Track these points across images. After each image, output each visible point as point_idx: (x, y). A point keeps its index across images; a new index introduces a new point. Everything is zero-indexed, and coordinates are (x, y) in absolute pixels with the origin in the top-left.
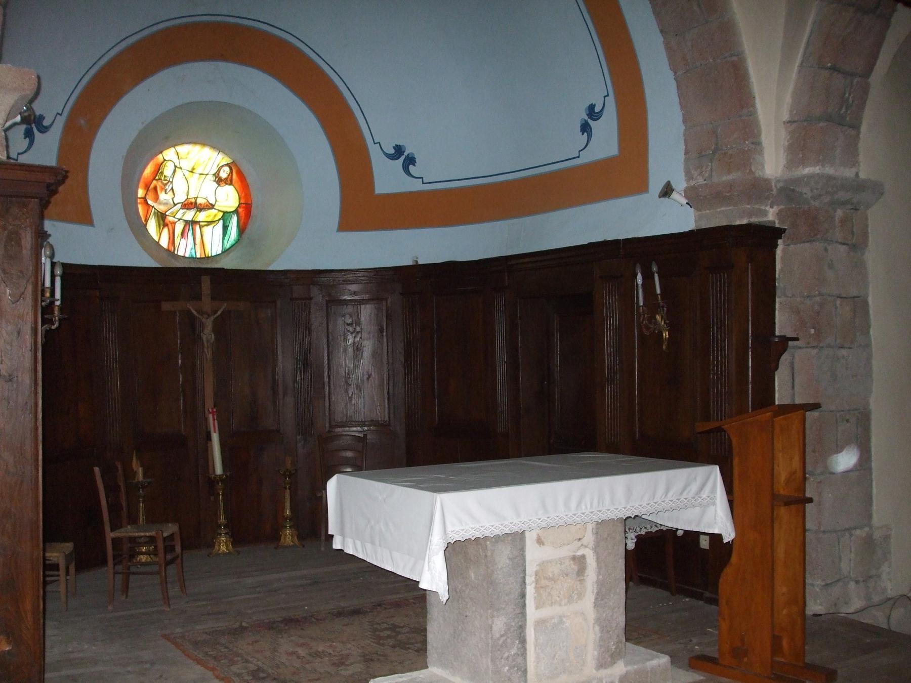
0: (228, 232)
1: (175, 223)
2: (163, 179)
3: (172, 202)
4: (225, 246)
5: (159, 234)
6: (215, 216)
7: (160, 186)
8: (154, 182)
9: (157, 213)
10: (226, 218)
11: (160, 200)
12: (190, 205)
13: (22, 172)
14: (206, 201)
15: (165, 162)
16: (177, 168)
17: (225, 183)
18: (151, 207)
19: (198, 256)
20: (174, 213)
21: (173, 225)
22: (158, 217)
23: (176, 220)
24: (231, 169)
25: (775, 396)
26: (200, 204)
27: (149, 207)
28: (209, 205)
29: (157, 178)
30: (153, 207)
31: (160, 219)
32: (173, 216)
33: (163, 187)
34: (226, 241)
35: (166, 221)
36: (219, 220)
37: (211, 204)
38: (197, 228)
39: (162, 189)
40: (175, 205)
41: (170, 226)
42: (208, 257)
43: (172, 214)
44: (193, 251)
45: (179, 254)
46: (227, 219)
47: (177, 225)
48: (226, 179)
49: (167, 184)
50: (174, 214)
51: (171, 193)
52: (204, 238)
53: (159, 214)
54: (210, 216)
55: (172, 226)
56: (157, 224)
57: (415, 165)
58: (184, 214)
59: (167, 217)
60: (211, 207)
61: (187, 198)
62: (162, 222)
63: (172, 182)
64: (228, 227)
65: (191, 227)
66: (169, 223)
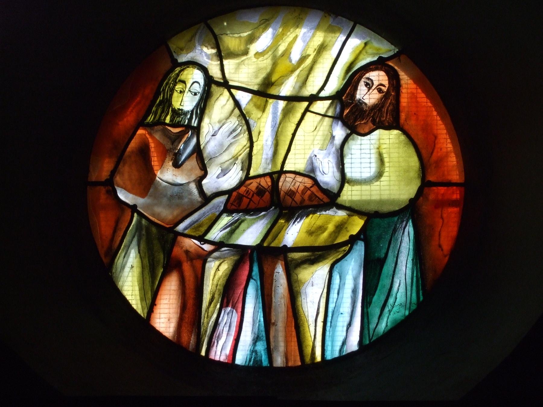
0: (384, 281)
1: (204, 258)
2: (168, 120)
3: (195, 191)
4: (372, 326)
5: (149, 296)
6: (340, 227)
7: (159, 144)
8: (141, 132)
9: (148, 230)
10: (374, 234)
11: (156, 188)
12: (256, 198)
13: (257, 330)
14: (308, 182)
15: (178, 70)
16: (214, 87)
17: (374, 122)
18: (128, 212)
19: (279, 361)
20: (200, 226)
21: (198, 264)
22: (149, 243)
23: (207, 247)
24: (393, 77)
25: (201, 321)
26: (291, 193)
27: (123, 211)
28: (320, 195)
29: (150, 119)
30: (134, 208)
31: (157, 245)
32: (199, 233)
33: (169, 146)
34: (375, 310)
35: (177, 251)
36: (353, 240)
37: (326, 192)
38: (280, 270)
39: (164, 153)
40: (206, 199)
41: (187, 267)
42: (314, 365)
43: (197, 228)
44: (261, 347)
45: (212, 356)
46: (380, 238)
47: (212, 266)
48: (377, 107)
49: (180, 136)
50: (203, 229)
51: (193, 163)
52: (366, 168)
53: (154, 230)
54: (322, 229)
55: (193, 267)
56: (146, 261)
57: (322, 322)
58: (234, 228)
59: (180, 238)
60: (326, 200)
61: (247, 177)
62: (161, 257)
63: (197, 131)
64: (382, 262)
65: (256, 269)
66: (183, 257)
